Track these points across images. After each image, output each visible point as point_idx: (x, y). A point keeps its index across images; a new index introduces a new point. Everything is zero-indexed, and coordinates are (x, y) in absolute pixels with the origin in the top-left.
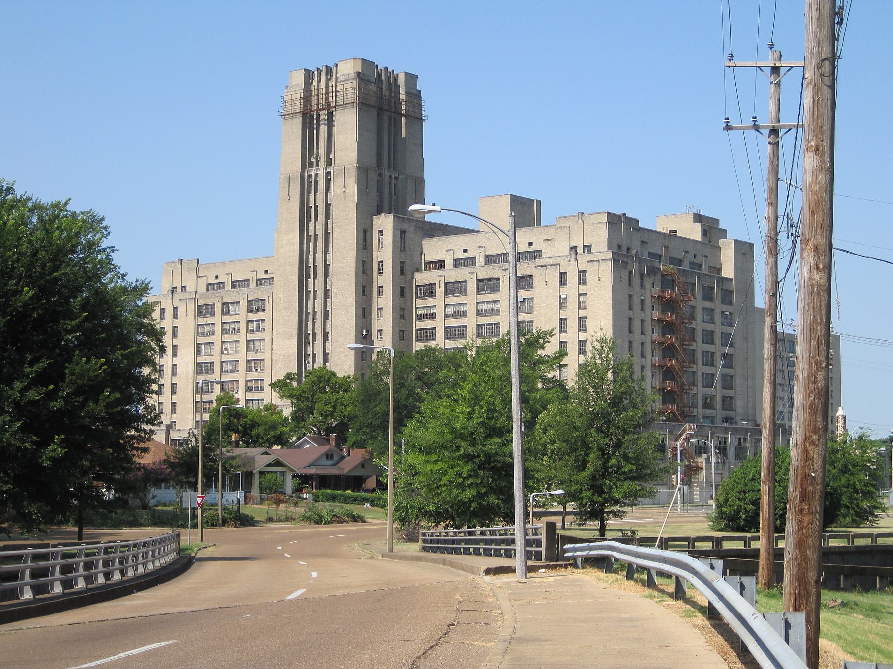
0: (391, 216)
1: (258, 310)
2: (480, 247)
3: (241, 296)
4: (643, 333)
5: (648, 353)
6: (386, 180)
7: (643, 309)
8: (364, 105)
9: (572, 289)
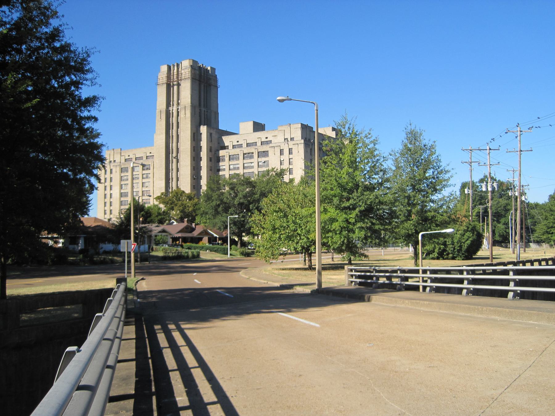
0: (206, 127)
1: (147, 169)
8: (194, 79)
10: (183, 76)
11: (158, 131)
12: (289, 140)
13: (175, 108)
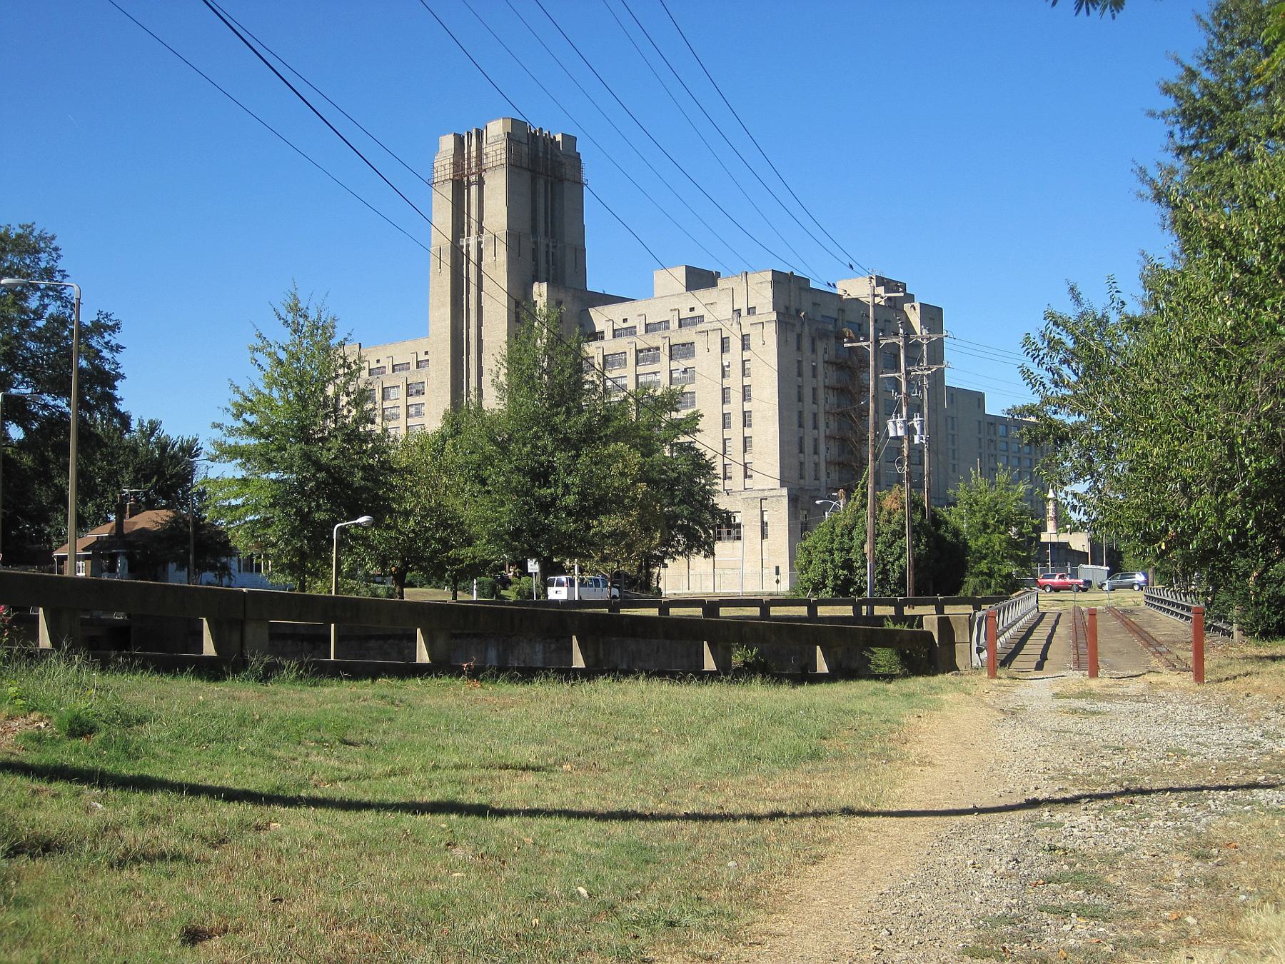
0: (545, 284)
1: (418, 392)
3: (400, 379)
5: (822, 447)
6: (543, 249)
7: (814, 376)
8: (514, 167)
10: (490, 160)
11: (433, 301)
12: (744, 313)
13: (473, 241)
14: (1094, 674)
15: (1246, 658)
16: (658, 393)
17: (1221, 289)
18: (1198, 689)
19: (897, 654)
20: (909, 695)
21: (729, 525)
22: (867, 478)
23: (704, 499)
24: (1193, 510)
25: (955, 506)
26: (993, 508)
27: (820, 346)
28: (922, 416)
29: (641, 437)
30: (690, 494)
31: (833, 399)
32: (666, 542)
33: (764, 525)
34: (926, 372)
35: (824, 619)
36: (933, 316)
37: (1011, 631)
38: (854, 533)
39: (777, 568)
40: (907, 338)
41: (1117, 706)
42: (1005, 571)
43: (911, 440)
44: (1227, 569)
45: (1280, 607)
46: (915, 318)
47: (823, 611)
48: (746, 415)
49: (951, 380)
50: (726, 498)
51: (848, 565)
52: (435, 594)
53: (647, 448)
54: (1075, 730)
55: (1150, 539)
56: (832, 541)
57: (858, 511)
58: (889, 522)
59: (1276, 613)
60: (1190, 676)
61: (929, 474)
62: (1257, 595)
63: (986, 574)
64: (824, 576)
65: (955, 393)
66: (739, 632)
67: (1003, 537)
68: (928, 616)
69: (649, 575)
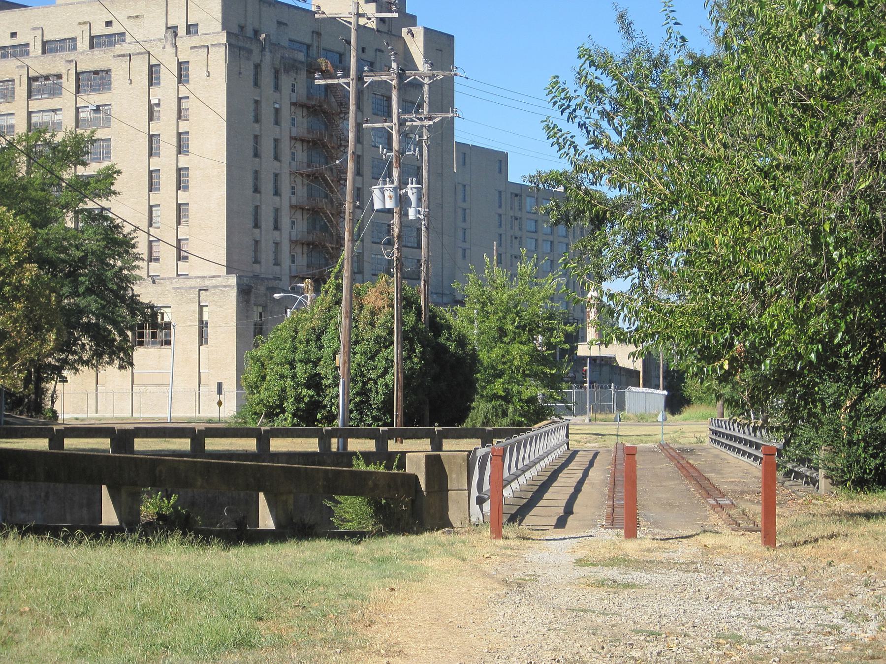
2: (34, 29)
4: (276, 158)
5: (285, 221)
7: (277, 123)
9: (167, 90)
12: (182, 31)
14: (631, 534)
15: (834, 514)
16: (58, 139)
17: (810, 25)
18: (767, 554)
19: (369, 504)
20: (382, 561)
21: (155, 325)
22: (342, 267)
23: (120, 288)
24: (766, 319)
25: (462, 304)
26: (512, 308)
27: (286, 81)
28: (419, 182)
29: (32, 200)
30: (101, 280)
31: (302, 155)
32: (65, 346)
33: (203, 326)
34: (427, 123)
35: (278, 456)
36: (441, 46)
37: (528, 474)
38: (324, 339)
39: (220, 385)
40: (401, 76)
41: (657, 577)
42: (526, 395)
43: (404, 214)
44: (809, 396)
45: (880, 448)
46: (416, 47)
47: (278, 445)
48: (181, 174)
49: (464, 134)
50: (151, 288)
51: (314, 382)
52: (231, 444)
53: (41, 216)
54: (598, 608)
55: (709, 356)
56: (294, 350)
57: (329, 309)
58: (372, 324)
59: (874, 456)
60: (757, 537)
61: (427, 262)
62: (850, 432)
63: (501, 397)
64: (282, 398)
65: (468, 152)
66: (158, 472)
67: (525, 348)
68: (415, 452)
69: (40, 392)
